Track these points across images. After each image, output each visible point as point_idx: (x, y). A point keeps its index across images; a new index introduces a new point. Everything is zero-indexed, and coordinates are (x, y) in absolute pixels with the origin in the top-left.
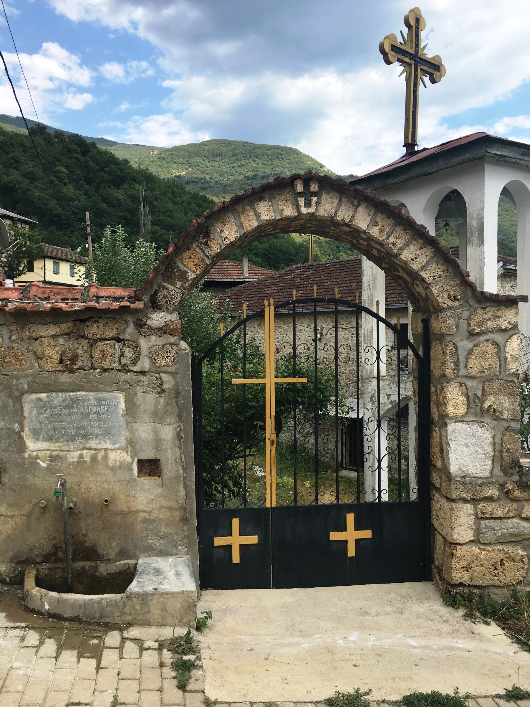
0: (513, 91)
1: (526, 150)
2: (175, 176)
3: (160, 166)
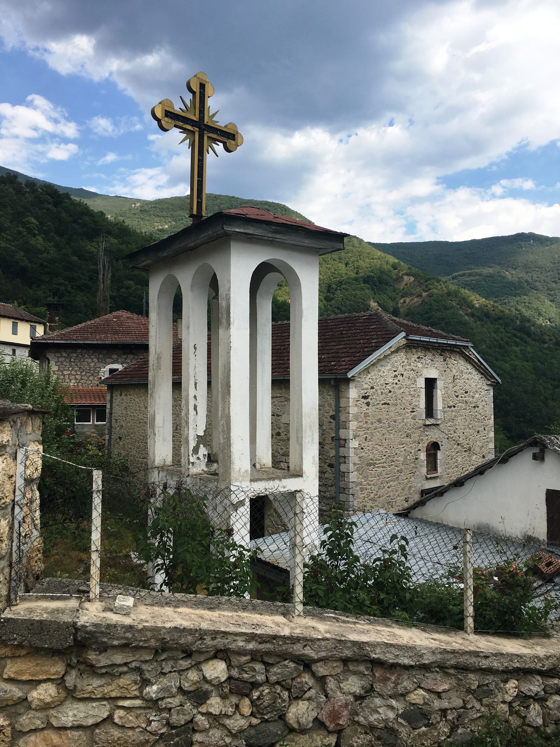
0: (508, 154)
1: (278, 228)
2: (157, 230)
3: (142, 219)
